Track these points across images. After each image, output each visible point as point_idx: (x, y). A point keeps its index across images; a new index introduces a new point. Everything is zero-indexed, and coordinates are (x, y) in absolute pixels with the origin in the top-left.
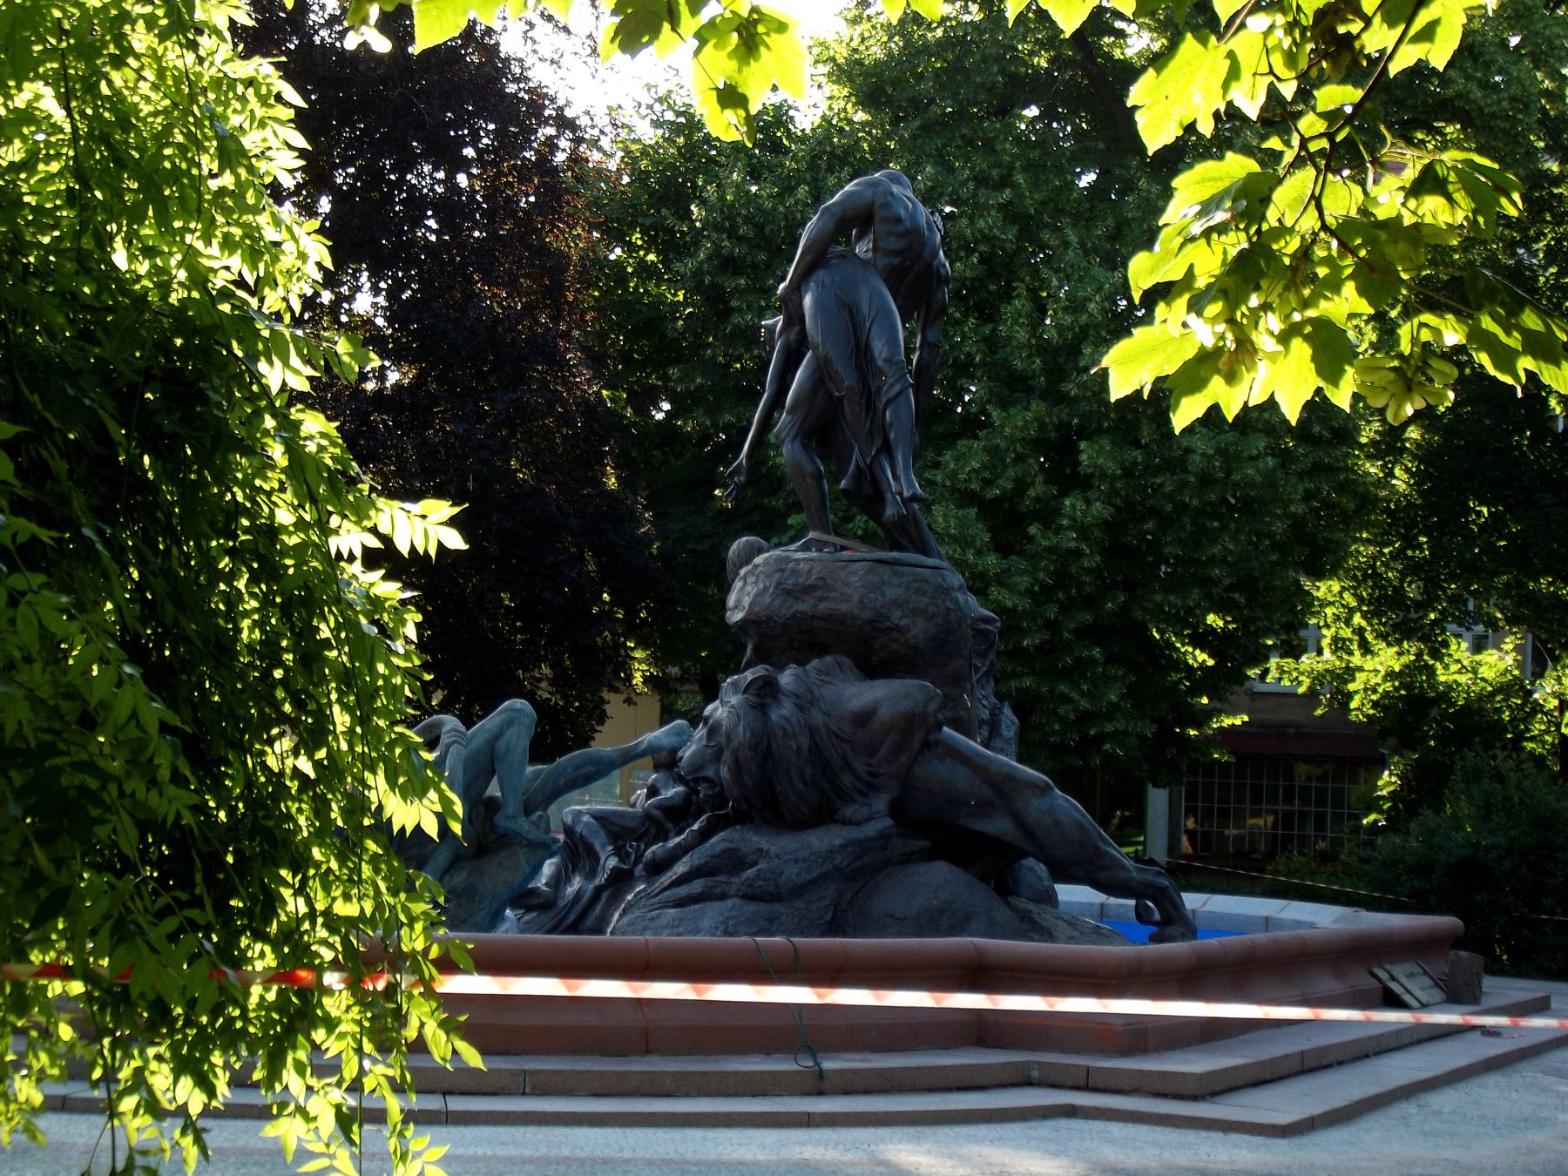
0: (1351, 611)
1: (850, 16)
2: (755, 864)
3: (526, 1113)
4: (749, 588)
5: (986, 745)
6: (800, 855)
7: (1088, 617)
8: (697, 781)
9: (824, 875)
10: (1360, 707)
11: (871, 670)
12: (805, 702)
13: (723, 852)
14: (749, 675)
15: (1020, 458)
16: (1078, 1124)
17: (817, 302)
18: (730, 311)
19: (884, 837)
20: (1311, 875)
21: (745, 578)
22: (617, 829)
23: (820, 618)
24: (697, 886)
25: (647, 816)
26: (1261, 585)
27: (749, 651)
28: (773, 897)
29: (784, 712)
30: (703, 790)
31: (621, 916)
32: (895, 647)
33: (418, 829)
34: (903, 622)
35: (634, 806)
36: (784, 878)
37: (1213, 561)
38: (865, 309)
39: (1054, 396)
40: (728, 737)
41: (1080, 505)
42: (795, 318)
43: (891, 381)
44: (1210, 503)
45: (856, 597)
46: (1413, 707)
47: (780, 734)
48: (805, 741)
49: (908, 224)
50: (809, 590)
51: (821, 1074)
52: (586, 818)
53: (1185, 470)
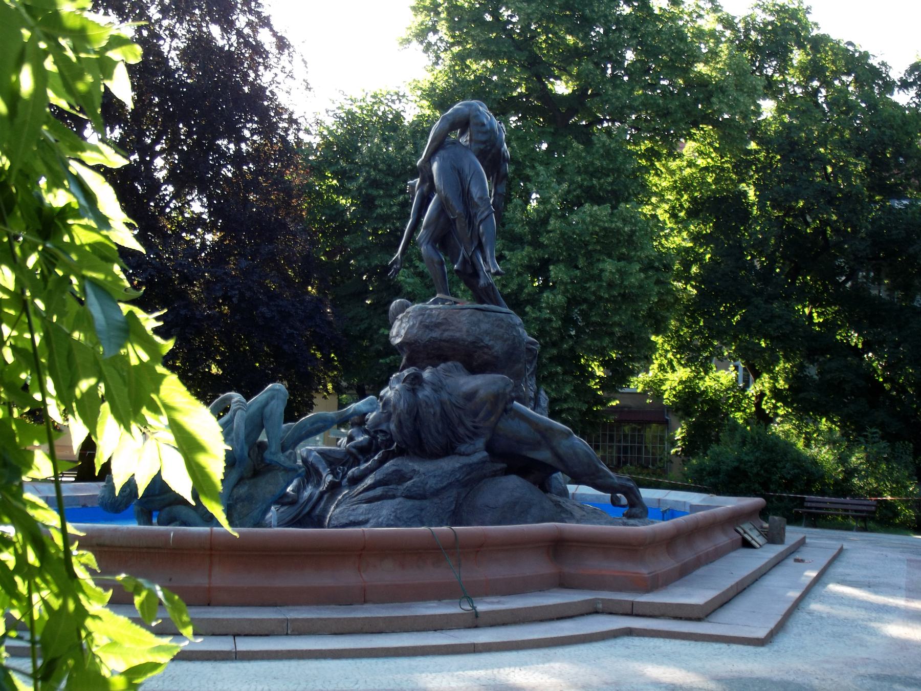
0: (667, 351)
1: (429, 68)
2: (411, 478)
3: (289, 651)
4: (404, 325)
5: (534, 409)
6: (437, 473)
7: (555, 352)
8: (376, 432)
9: (450, 484)
10: (668, 397)
11: (473, 370)
12: (438, 387)
13: (394, 471)
14: (406, 373)
15: (520, 274)
16: (636, 641)
17: (440, 168)
18: (376, 207)
19: (483, 462)
20: (639, 474)
21: (401, 319)
22: (332, 460)
23: (444, 341)
24: (378, 491)
25: (348, 452)
26: (636, 336)
27: (404, 360)
28: (423, 497)
29: (426, 393)
30: (380, 437)
31: (335, 508)
32: (486, 357)
33: (158, 485)
34: (491, 343)
35: (340, 446)
36: (428, 486)
37: (615, 324)
38: (467, 171)
39: (536, 244)
40: (395, 407)
41: (551, 296)
42: (428, 178)
43: (482, 209)
44: (614, 296)
45: (464, 329)
46: (690, 397)
47: (424, 405)
48: (438, 409)
49: (488, 127)
50: (437, 325)
51: (477, 615)
52: (315, 453)
53: (601, 280)
